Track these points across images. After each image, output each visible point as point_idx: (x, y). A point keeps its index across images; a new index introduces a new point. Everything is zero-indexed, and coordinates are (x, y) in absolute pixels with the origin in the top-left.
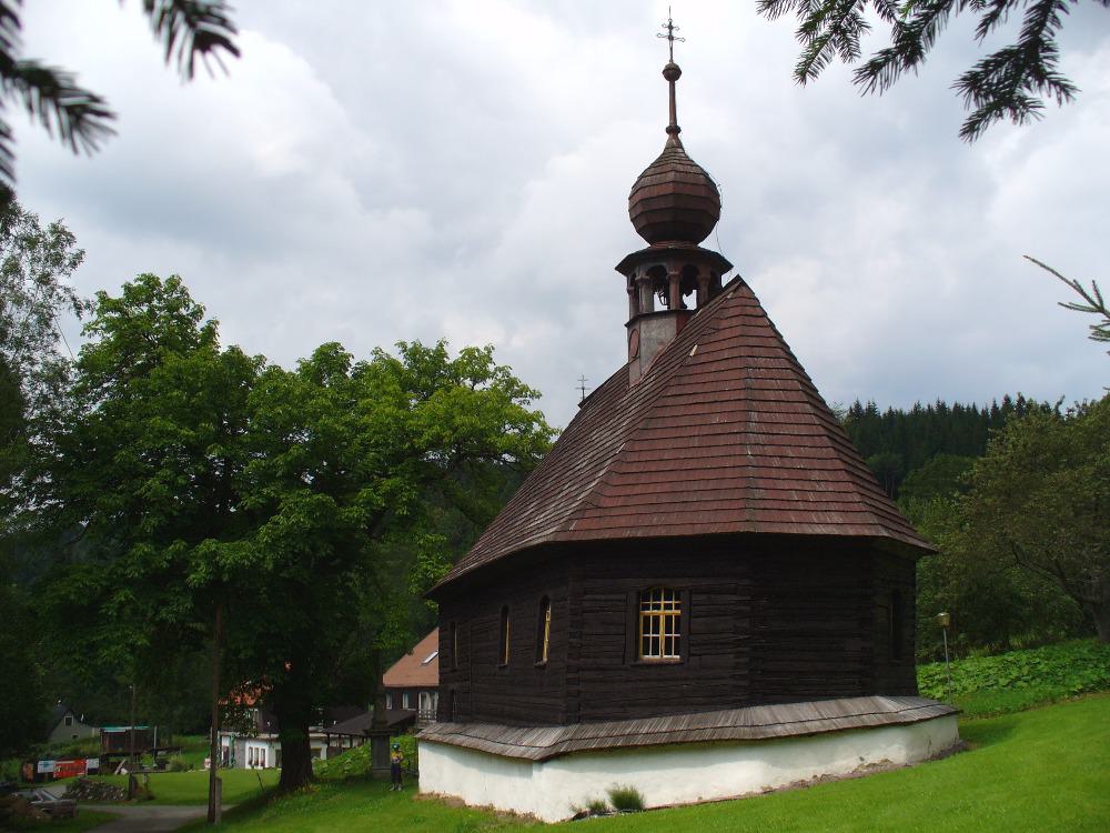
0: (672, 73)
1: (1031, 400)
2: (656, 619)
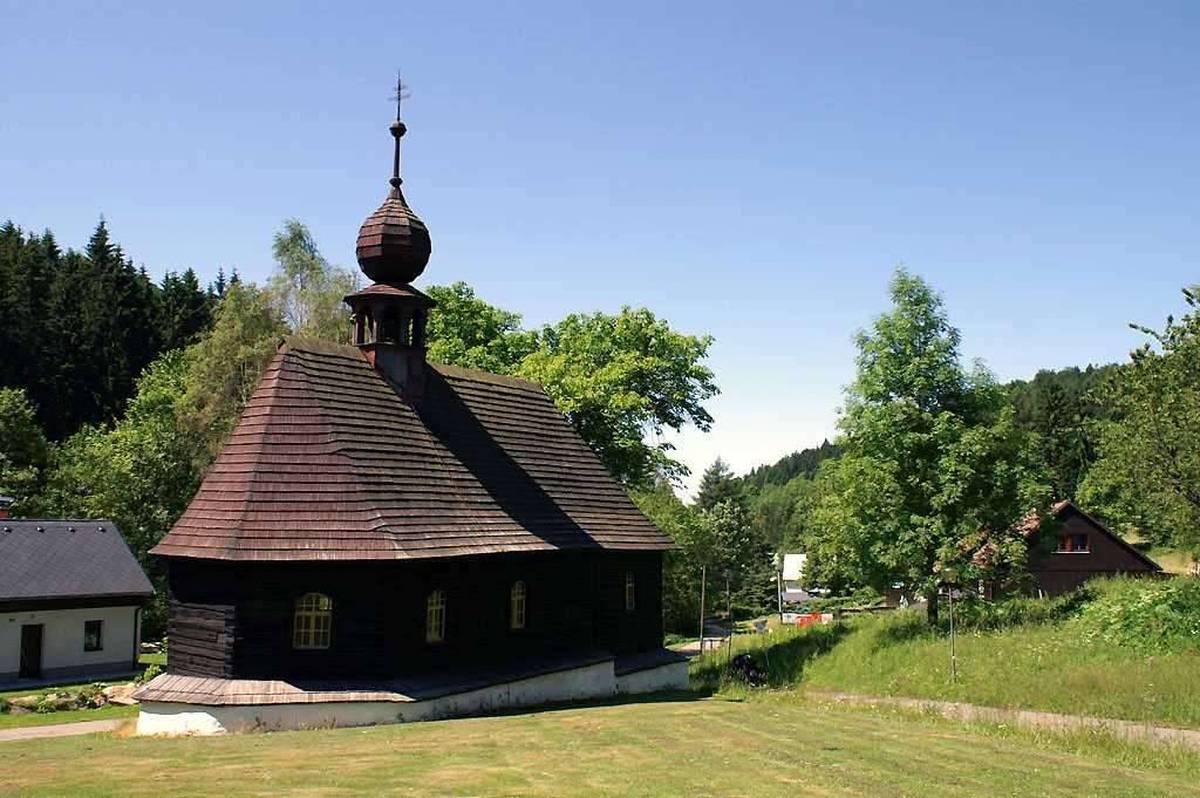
0: (398, 131)
2: (308, 619)
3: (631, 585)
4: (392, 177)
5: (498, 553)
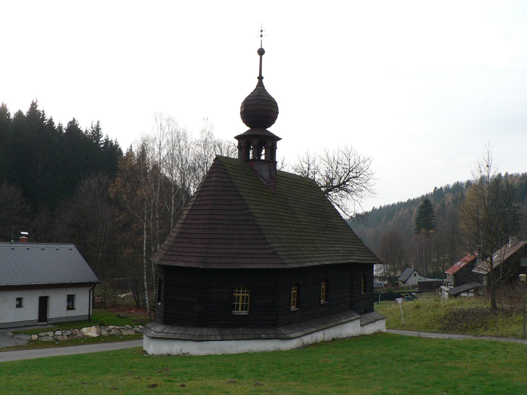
0: (261, 52)
1: (507, 174)
2: (238, 297)
3: (295, 291)
4: (258, 75)
5: (321, 265)
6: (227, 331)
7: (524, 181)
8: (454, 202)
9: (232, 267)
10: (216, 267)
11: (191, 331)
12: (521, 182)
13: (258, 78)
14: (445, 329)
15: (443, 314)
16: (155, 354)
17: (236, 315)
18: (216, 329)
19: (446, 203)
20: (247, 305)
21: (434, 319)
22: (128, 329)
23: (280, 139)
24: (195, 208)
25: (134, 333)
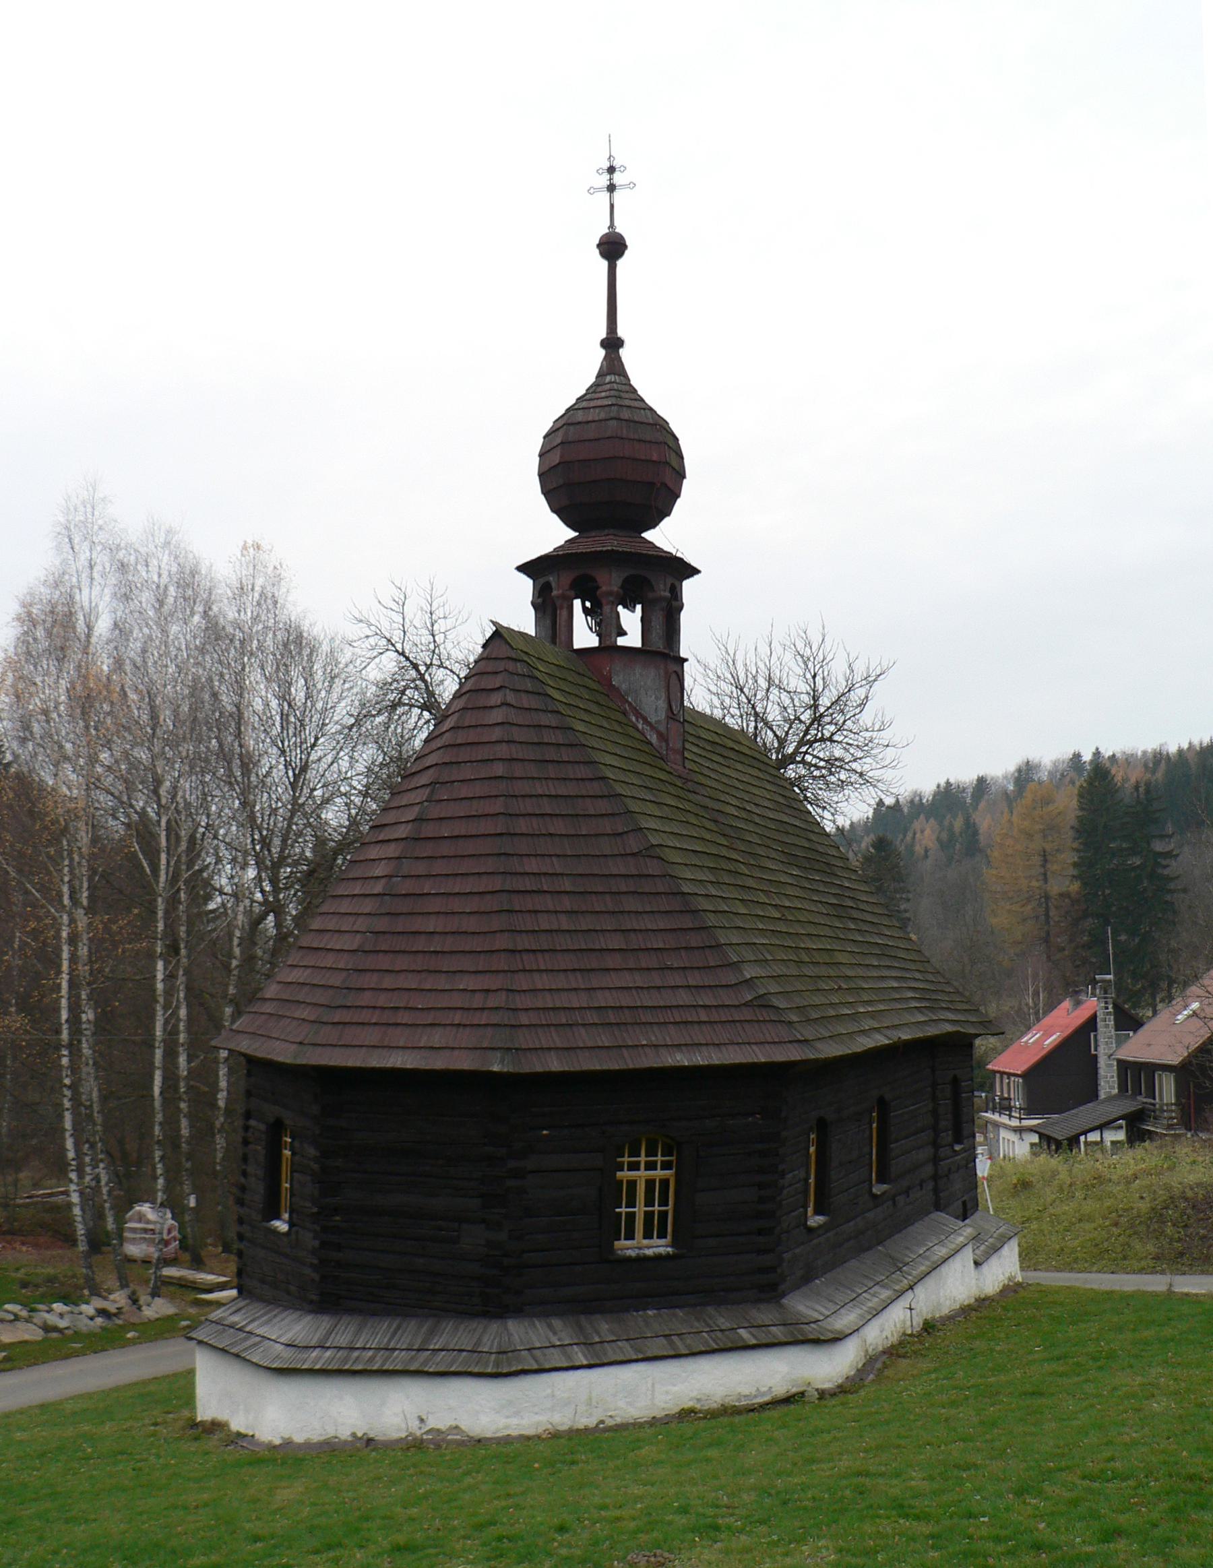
0: (612, 247)
1: (1097, 753)
2: (632, 1184)
4: (603, 334)
6: (604, 1327)
7: (1159, 775)
8: (946, 845)
9: (615, 1066)
10: (555, 1064)
11: (456, 1335)
12: (1148, 775)
13: (604, 344)
14: (1180, 1258)
15: (1144, 1206)
16: (299, 1438)
17: (629, 1259)
18: (557, 1323)
19: (919, 849)
20: (663, 1215)
21: (1116, 1224)
22: (17, 1318)
23: (694, 571)
24: (429, 830)
25: (38, 1335)
